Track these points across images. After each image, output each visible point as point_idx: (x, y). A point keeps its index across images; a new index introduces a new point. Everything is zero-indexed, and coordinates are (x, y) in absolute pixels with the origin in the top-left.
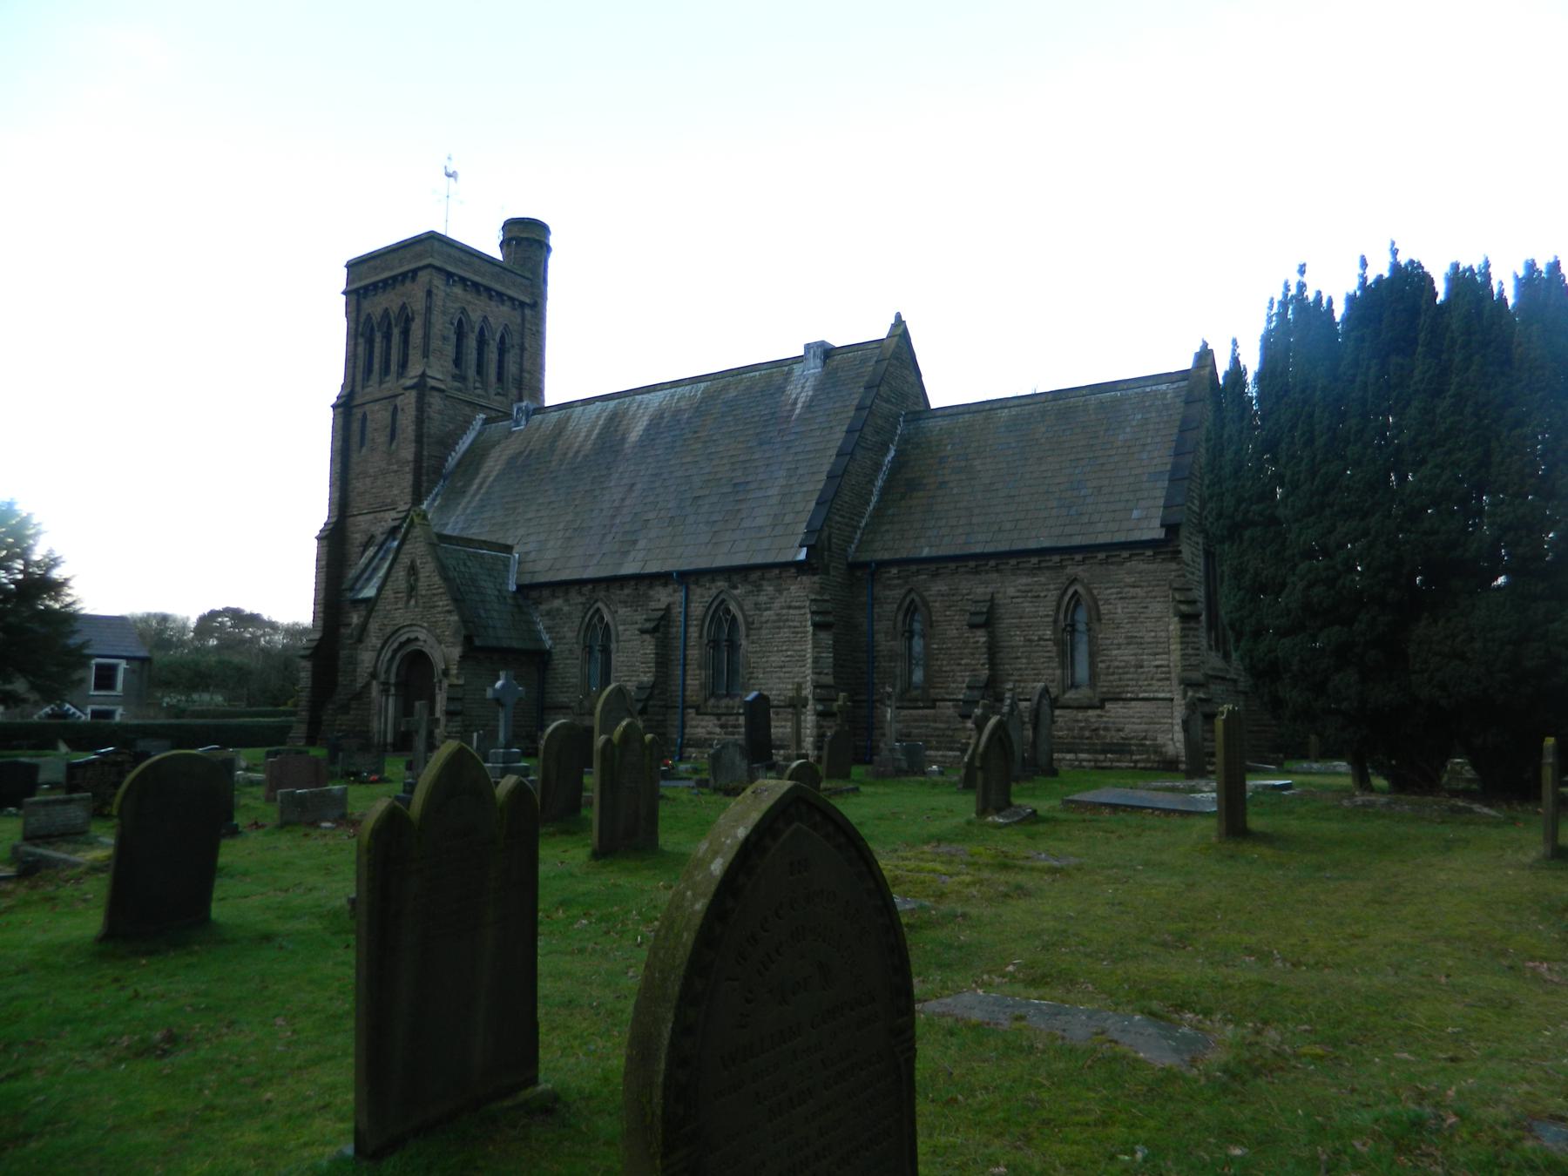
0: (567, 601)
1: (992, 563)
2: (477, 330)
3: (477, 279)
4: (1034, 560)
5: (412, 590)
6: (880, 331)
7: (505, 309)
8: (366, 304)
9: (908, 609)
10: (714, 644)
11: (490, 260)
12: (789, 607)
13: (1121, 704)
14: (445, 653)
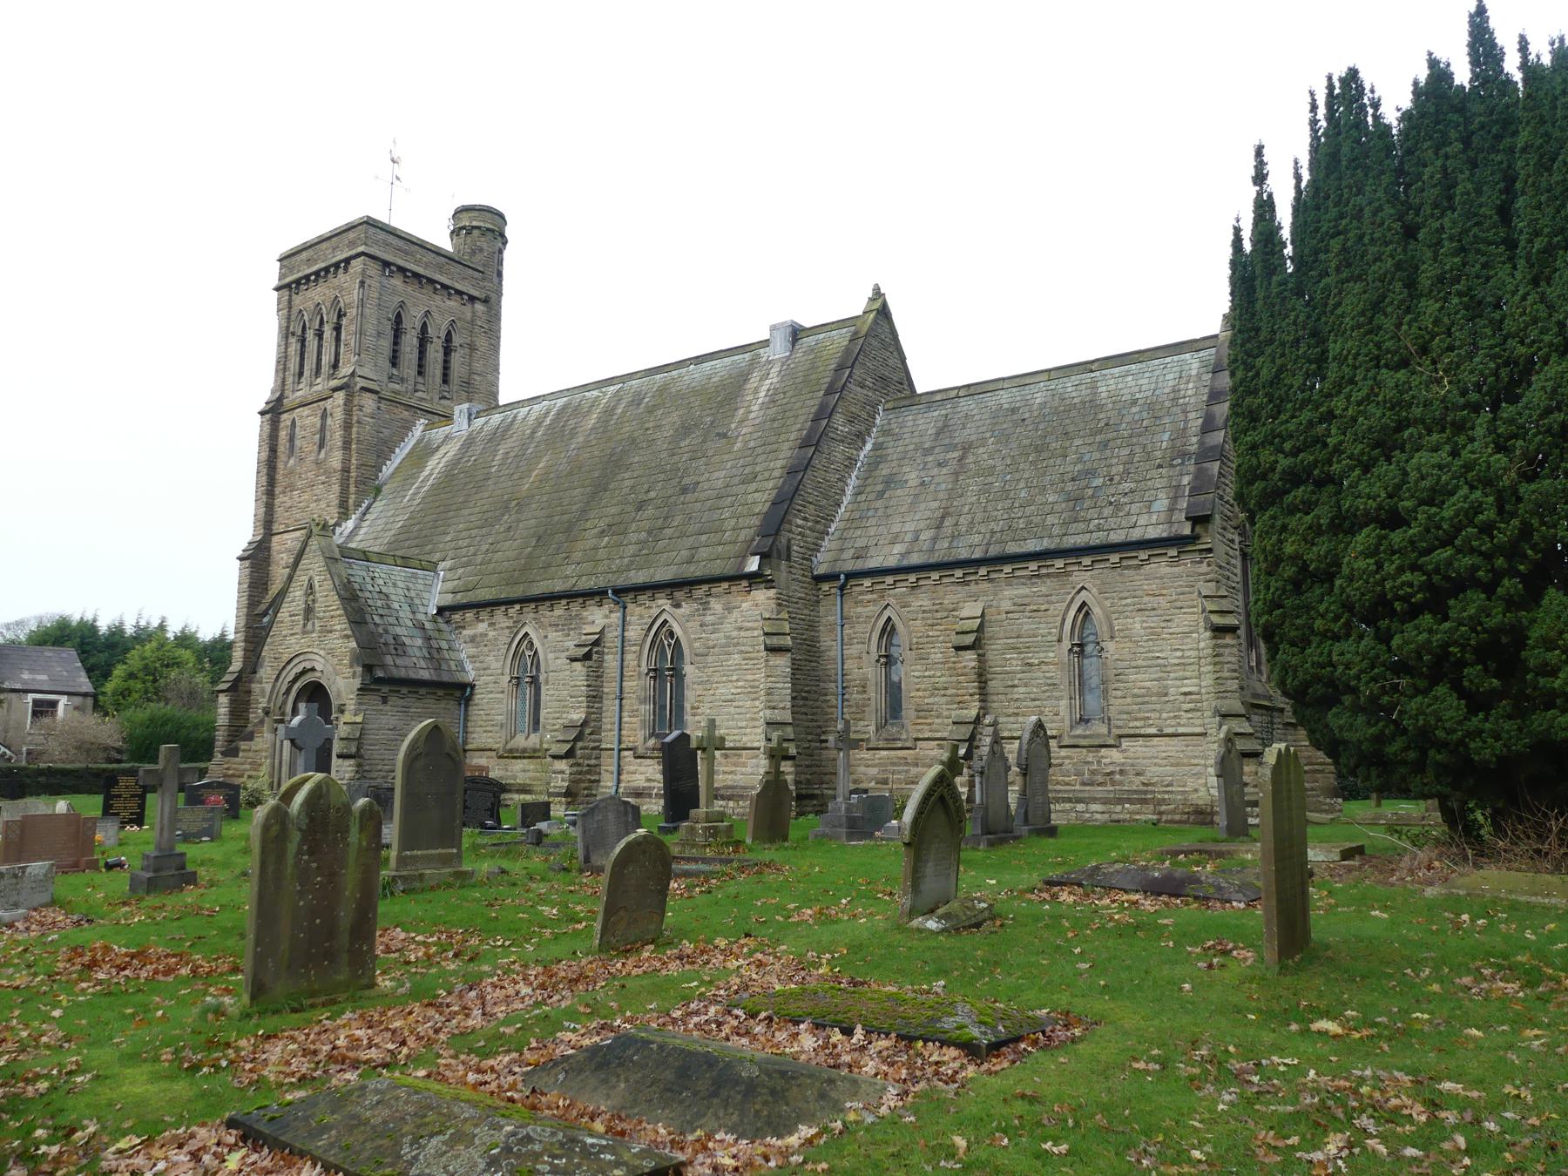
0: (491, 624)
1: (983, 571)
2: (418, 325)
3: (420, 270)
4: (1033, 566)
5: (309, 611)
6: (854, 305)
7: (453, 304)
8: (297, 300)
9: (884, 630)
10: (656, 673)
11: (438, 252)
12: (740, 629)
13: (1141, 741)
14: (343, 684)
